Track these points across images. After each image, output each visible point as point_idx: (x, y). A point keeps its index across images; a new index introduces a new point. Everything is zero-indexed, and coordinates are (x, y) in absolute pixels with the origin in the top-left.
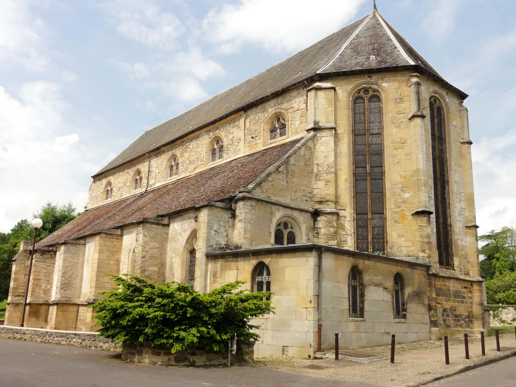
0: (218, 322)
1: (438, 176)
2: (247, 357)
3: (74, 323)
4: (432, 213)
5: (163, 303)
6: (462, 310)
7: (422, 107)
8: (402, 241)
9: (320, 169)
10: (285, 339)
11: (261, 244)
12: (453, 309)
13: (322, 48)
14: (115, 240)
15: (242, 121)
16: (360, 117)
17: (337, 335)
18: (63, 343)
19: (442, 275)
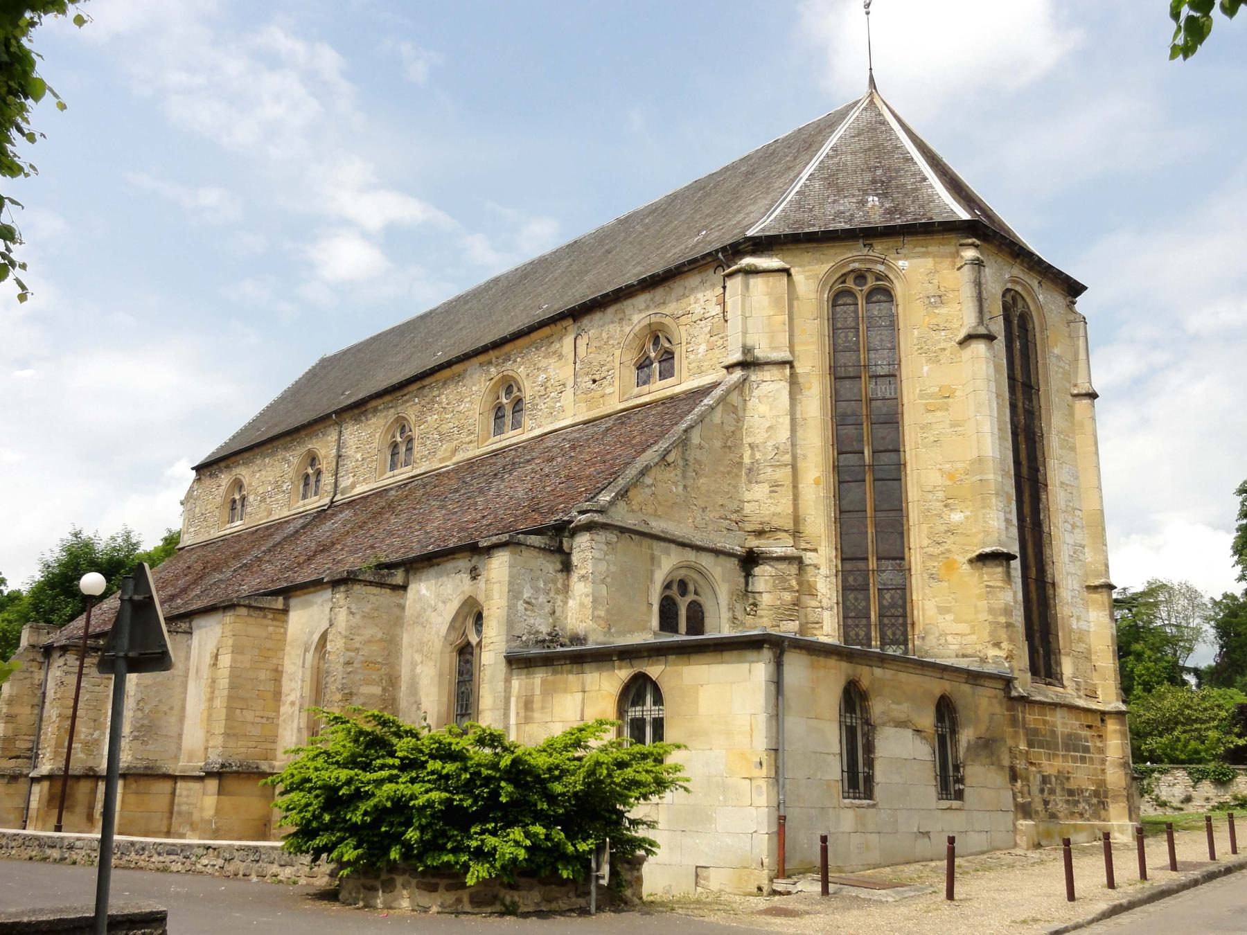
0: (567, 813)
1: (1025, 471)
2: (628, 893)
3: (165, 822)
4: (1014, 557)
5: (444, 772)
6: (1082, 777)
7: (987, 316)
8: (946, 623)
9: (758, 456)
10: (700, 849)
11: (631, 632)
12: (1063, 777)
13: (753, 173)
14: (269, 622)
15: (568, 341)
16: (846, 336)
17: (824, 839)
18: (174, 867)
19: (1038, 698)
